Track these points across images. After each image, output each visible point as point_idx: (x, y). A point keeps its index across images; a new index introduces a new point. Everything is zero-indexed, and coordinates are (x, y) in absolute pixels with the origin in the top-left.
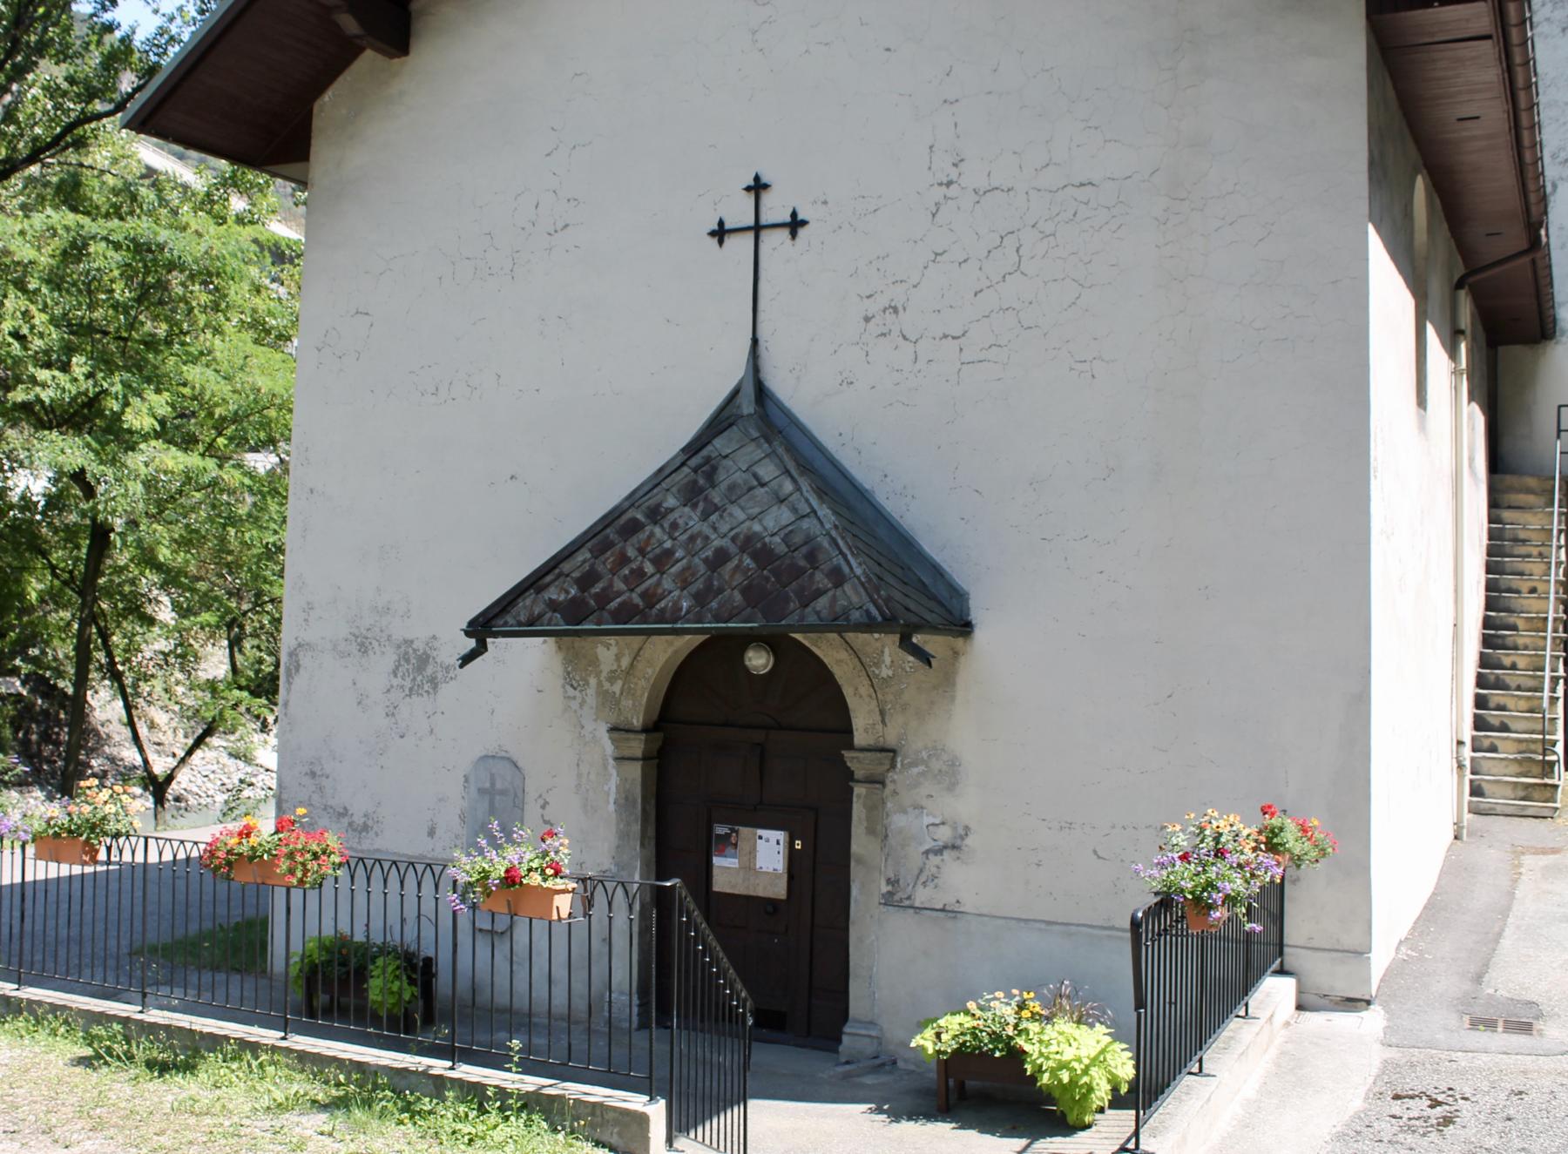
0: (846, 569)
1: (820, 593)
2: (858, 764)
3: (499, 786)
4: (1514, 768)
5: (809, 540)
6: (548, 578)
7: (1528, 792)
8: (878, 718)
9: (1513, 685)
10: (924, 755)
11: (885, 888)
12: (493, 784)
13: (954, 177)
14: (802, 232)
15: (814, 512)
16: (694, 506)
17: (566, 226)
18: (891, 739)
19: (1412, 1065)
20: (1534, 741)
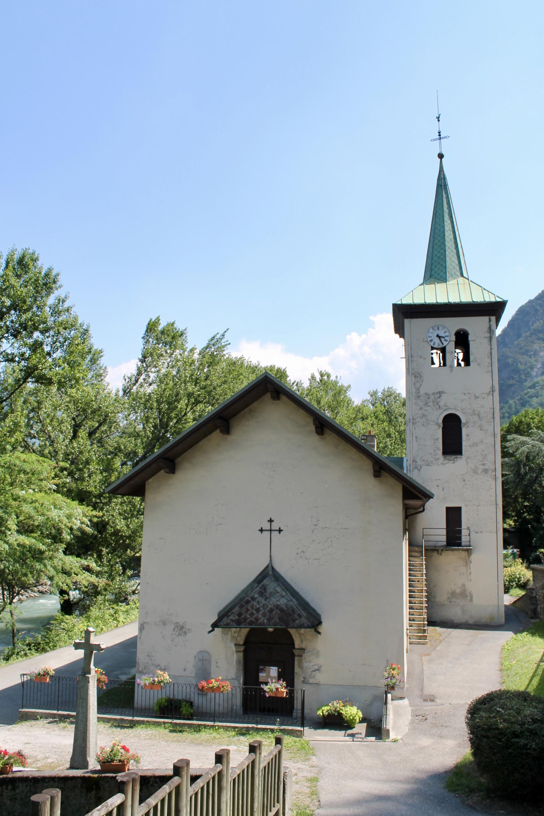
0: (301, 614)
1: (296, 619)
2: (296, 652)
3: (205, 658)
4: (417, 631)
5: (291, 607)
6: (230, 614)
7: (420, 638)
8: (301, 642)
9: (415, 608)
10: (311, 650)
11: (302, 679)
12: (203, 657)
13: (317, 524)
14: (282, 532)
15: (291, 600)
16: (262, 597)
17: (221, 524)
18: (304, 647)
19: (417, 710)
20: (422, 624)
